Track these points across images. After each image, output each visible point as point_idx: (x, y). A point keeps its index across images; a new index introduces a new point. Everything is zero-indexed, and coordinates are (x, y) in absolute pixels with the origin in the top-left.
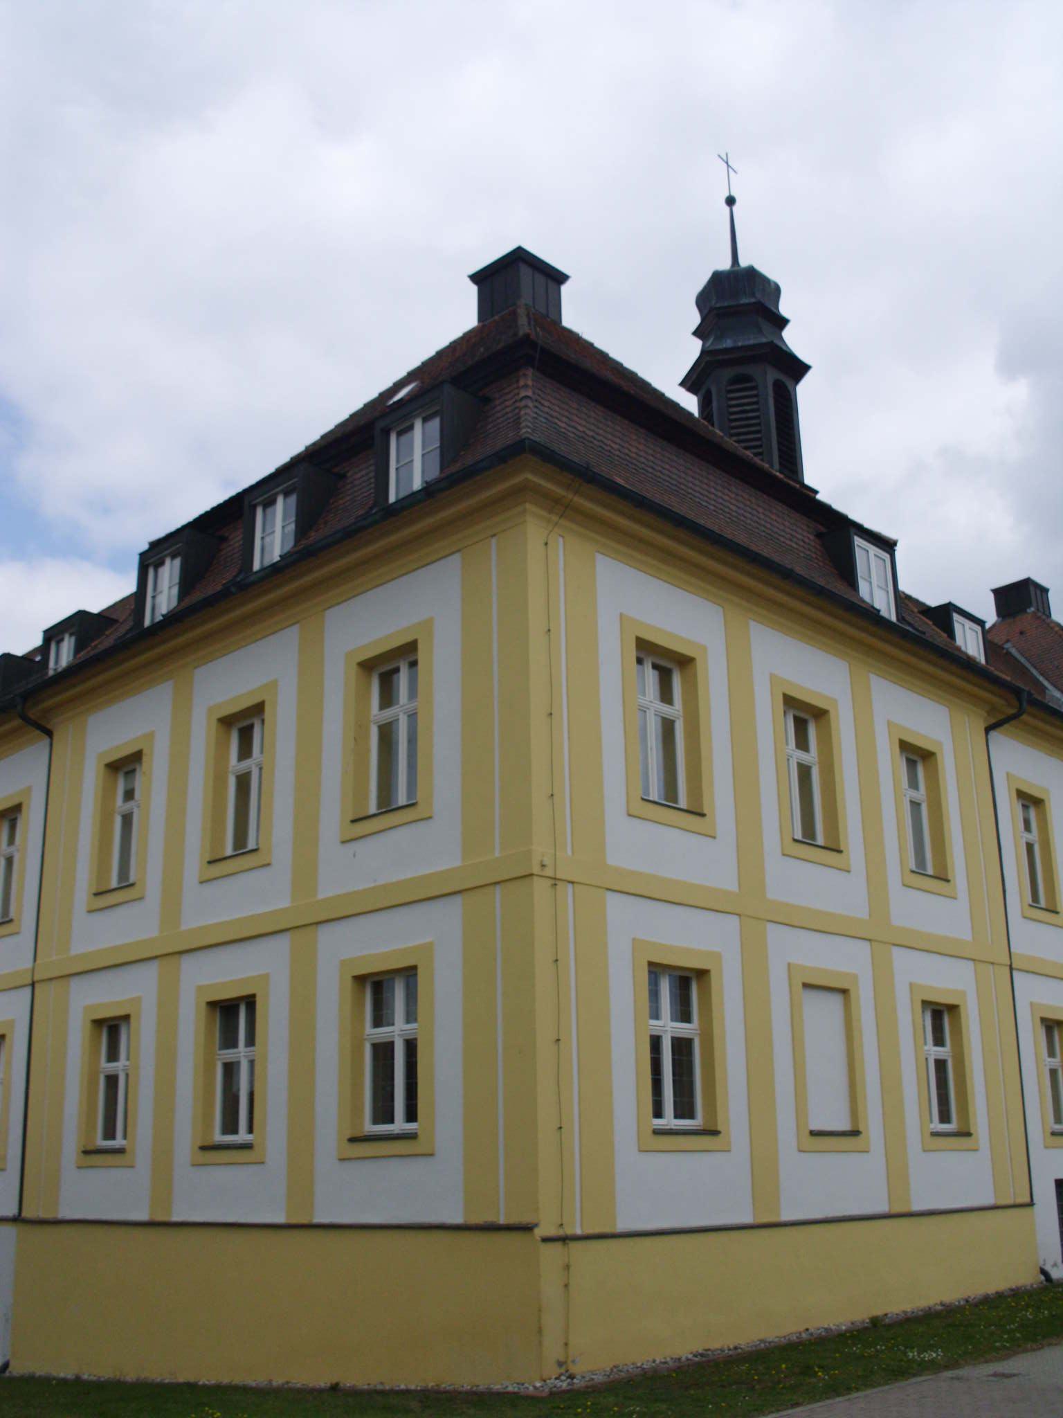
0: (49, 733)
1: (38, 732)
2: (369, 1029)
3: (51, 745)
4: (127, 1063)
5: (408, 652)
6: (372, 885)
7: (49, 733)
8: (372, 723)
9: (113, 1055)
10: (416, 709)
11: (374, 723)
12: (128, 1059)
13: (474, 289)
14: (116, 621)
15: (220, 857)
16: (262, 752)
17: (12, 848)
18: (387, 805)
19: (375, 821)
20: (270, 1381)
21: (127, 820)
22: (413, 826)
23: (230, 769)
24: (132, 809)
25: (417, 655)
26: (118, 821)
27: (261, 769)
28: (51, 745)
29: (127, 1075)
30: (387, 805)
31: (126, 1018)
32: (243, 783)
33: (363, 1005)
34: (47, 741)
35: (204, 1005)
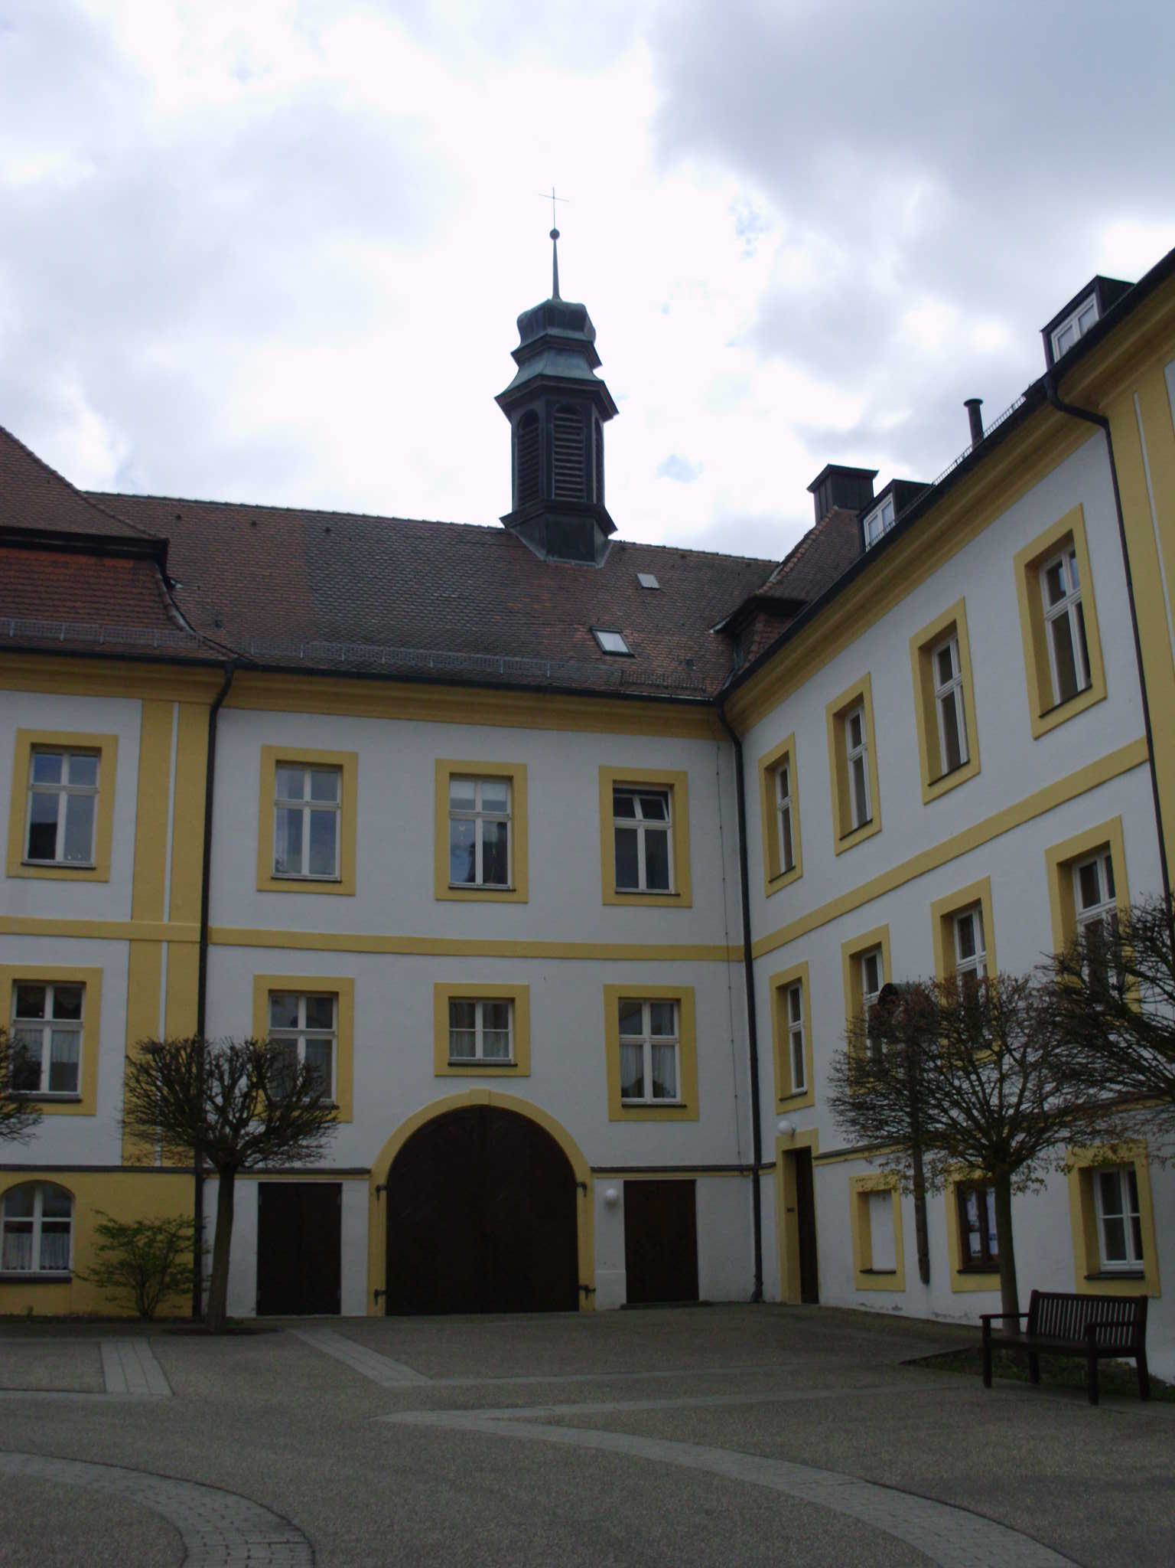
0: (1103, 422)
1: (1088, 424)
2: (791, 1024)
3: (1109, 435)
4: (984, 953)
5: (1065, 543)
6: (950, 837)
7: (1103, 422)
8: (1046, 622)
9: (968, 950)
10: (1080, 598)
11: (939, 698)
12: (984, 949)
13: (811, 496)
14: (807, 602)
15: (1050, 708)
16: (960, 671)
17: (859, 748)
18: (955, 765)
19: (1061, 710)
20: (31, 1309)
21: (859, 764)
22: (1093, 710)
23: (936, 694)
24: (861, 753)
25: (1073, 546)
26: (780, 816)
27: (962, 687)
28: (1109, 435)
29: (985, 967)
30: (1070, 693)
31: (977, 904)
32: (949, 702)
33: (953, 943)
34: (1102, 432)
35: (1055, 868)
